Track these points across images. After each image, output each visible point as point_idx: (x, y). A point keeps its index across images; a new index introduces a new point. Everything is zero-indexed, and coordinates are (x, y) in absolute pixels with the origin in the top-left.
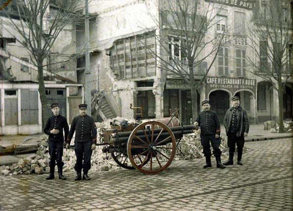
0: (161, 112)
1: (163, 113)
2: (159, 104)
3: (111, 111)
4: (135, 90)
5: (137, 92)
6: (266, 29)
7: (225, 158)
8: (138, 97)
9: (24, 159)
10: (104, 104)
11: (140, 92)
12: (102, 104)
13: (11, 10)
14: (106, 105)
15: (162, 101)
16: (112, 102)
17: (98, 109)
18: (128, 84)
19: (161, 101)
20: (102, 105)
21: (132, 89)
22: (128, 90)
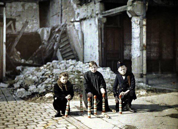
0: (142, 50)
1: (145, 52)
2: (138, 35)
3: (73, 54)
4: (100, 16)
5: (105, 20)
6: (51, 85)
7: (120, 111)
8: (105, 28)
9: (95, 69)
10: (63, 42)
11: (110, 18)
12: (62, 41)
13: (39, 105)
14: (67, 43)
15: (144, 29)
16: (74, 39)
17: (57, 49)
18: (92, 8)
19: (141, 28)
20: (61, 44)
21: (97, 14)
22: (91, 17)
